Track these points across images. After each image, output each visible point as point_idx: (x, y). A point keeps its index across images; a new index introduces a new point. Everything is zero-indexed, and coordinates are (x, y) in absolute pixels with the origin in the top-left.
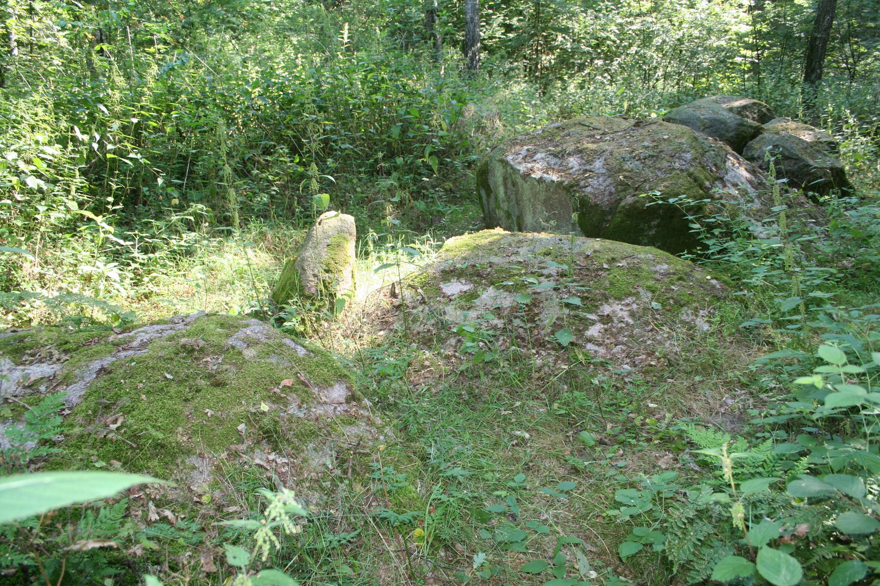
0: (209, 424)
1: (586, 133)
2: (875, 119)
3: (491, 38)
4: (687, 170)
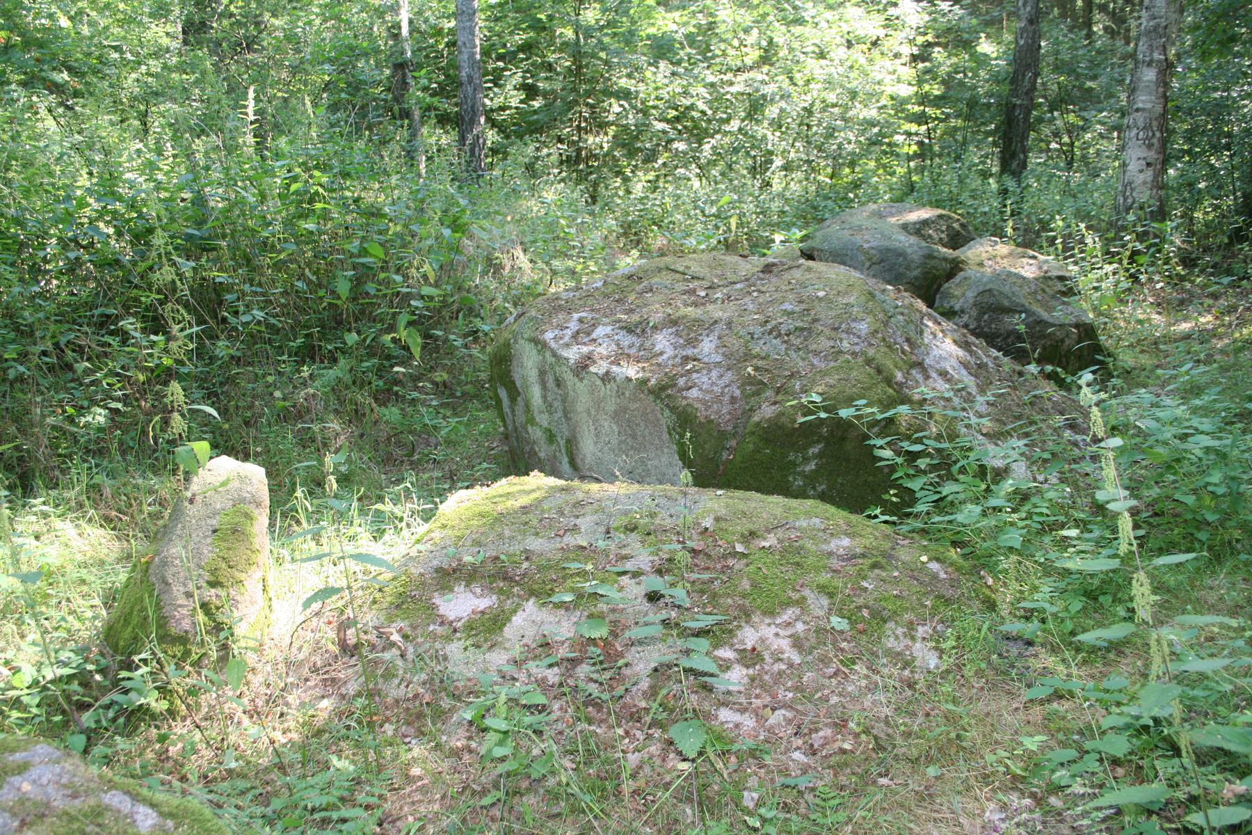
1: (681, 287)
2: (1128, 238)
3: (502, 109)
4: (864, 353)
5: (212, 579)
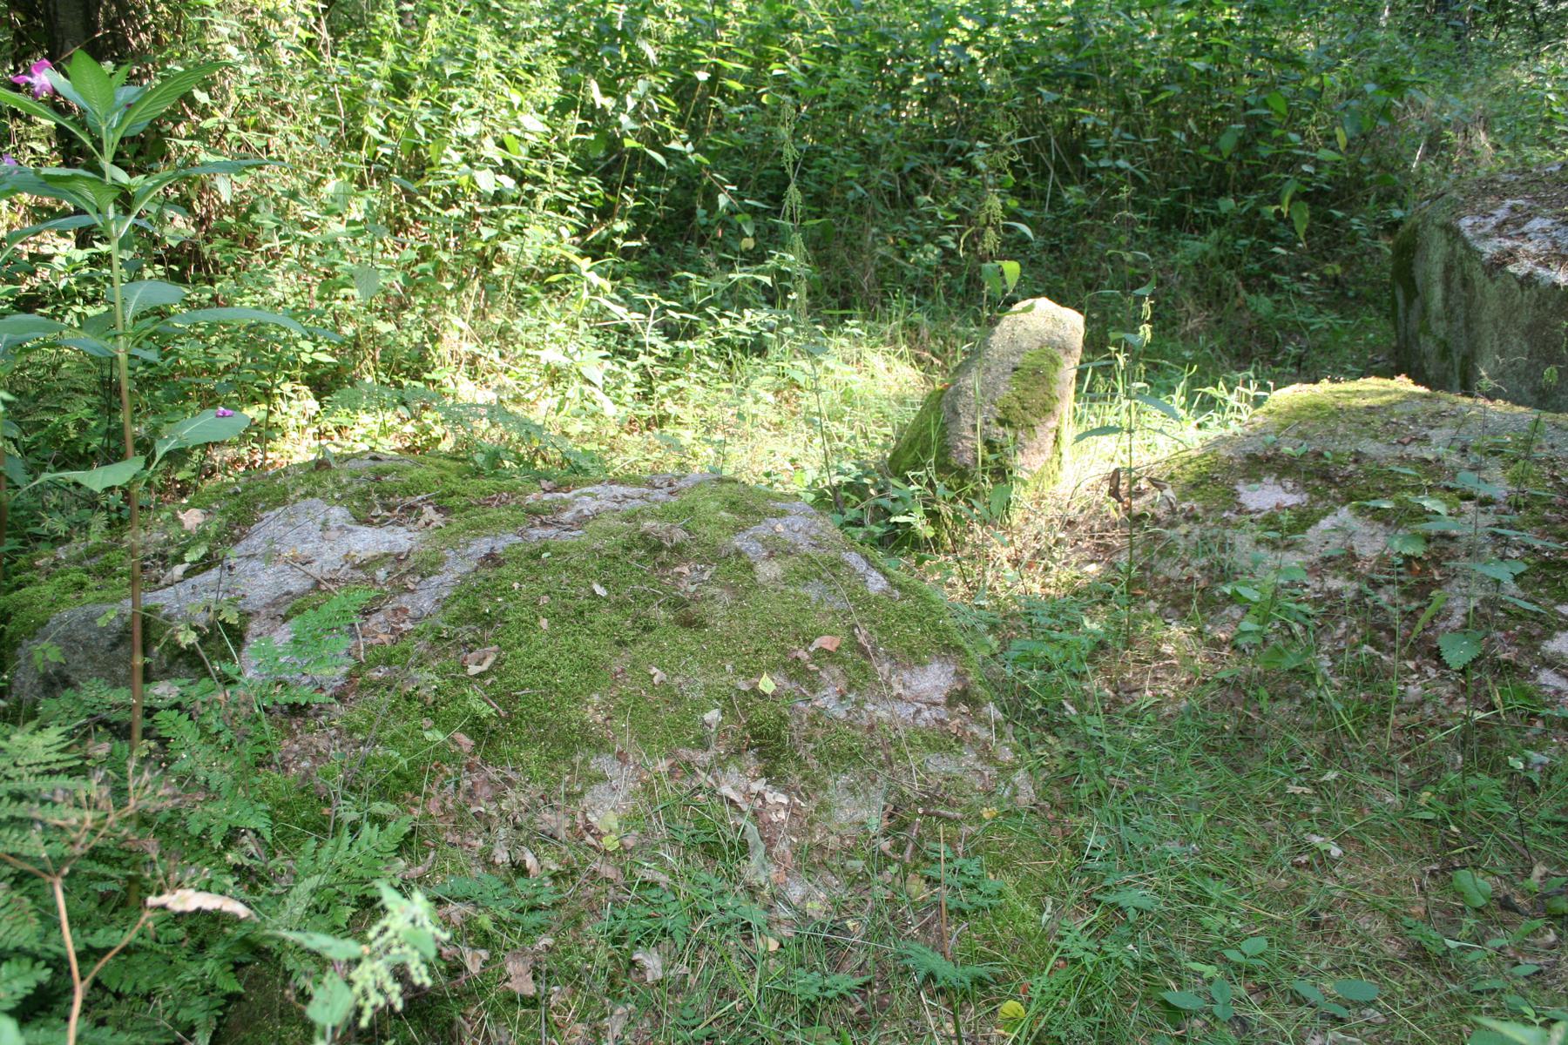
0: (651, 698)
5: (1003, 416)
